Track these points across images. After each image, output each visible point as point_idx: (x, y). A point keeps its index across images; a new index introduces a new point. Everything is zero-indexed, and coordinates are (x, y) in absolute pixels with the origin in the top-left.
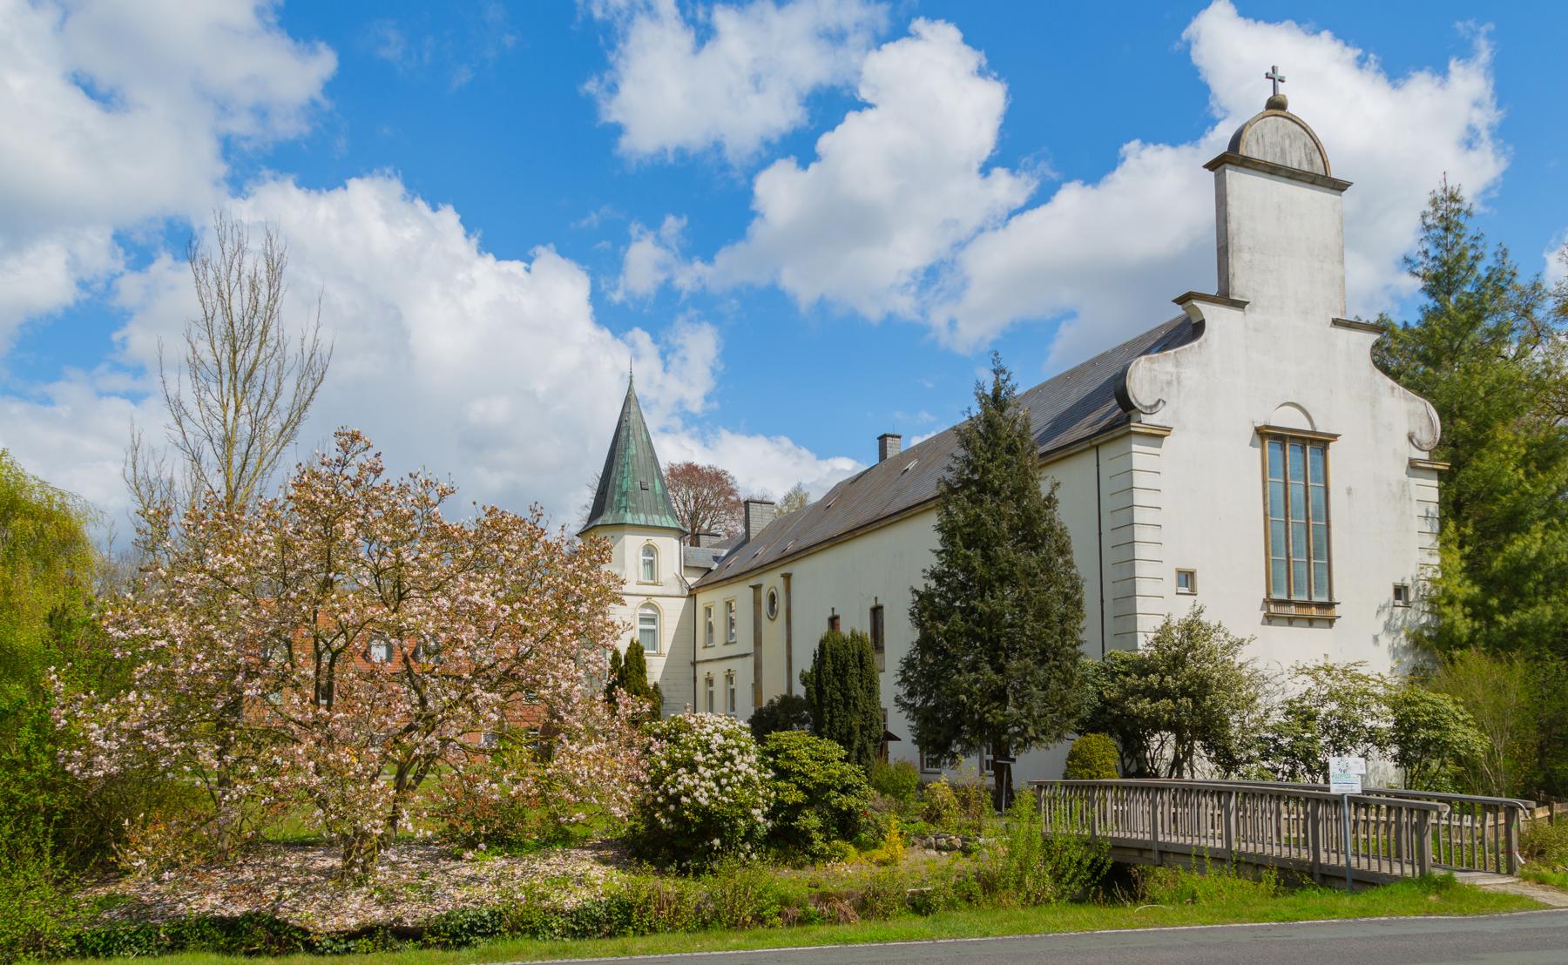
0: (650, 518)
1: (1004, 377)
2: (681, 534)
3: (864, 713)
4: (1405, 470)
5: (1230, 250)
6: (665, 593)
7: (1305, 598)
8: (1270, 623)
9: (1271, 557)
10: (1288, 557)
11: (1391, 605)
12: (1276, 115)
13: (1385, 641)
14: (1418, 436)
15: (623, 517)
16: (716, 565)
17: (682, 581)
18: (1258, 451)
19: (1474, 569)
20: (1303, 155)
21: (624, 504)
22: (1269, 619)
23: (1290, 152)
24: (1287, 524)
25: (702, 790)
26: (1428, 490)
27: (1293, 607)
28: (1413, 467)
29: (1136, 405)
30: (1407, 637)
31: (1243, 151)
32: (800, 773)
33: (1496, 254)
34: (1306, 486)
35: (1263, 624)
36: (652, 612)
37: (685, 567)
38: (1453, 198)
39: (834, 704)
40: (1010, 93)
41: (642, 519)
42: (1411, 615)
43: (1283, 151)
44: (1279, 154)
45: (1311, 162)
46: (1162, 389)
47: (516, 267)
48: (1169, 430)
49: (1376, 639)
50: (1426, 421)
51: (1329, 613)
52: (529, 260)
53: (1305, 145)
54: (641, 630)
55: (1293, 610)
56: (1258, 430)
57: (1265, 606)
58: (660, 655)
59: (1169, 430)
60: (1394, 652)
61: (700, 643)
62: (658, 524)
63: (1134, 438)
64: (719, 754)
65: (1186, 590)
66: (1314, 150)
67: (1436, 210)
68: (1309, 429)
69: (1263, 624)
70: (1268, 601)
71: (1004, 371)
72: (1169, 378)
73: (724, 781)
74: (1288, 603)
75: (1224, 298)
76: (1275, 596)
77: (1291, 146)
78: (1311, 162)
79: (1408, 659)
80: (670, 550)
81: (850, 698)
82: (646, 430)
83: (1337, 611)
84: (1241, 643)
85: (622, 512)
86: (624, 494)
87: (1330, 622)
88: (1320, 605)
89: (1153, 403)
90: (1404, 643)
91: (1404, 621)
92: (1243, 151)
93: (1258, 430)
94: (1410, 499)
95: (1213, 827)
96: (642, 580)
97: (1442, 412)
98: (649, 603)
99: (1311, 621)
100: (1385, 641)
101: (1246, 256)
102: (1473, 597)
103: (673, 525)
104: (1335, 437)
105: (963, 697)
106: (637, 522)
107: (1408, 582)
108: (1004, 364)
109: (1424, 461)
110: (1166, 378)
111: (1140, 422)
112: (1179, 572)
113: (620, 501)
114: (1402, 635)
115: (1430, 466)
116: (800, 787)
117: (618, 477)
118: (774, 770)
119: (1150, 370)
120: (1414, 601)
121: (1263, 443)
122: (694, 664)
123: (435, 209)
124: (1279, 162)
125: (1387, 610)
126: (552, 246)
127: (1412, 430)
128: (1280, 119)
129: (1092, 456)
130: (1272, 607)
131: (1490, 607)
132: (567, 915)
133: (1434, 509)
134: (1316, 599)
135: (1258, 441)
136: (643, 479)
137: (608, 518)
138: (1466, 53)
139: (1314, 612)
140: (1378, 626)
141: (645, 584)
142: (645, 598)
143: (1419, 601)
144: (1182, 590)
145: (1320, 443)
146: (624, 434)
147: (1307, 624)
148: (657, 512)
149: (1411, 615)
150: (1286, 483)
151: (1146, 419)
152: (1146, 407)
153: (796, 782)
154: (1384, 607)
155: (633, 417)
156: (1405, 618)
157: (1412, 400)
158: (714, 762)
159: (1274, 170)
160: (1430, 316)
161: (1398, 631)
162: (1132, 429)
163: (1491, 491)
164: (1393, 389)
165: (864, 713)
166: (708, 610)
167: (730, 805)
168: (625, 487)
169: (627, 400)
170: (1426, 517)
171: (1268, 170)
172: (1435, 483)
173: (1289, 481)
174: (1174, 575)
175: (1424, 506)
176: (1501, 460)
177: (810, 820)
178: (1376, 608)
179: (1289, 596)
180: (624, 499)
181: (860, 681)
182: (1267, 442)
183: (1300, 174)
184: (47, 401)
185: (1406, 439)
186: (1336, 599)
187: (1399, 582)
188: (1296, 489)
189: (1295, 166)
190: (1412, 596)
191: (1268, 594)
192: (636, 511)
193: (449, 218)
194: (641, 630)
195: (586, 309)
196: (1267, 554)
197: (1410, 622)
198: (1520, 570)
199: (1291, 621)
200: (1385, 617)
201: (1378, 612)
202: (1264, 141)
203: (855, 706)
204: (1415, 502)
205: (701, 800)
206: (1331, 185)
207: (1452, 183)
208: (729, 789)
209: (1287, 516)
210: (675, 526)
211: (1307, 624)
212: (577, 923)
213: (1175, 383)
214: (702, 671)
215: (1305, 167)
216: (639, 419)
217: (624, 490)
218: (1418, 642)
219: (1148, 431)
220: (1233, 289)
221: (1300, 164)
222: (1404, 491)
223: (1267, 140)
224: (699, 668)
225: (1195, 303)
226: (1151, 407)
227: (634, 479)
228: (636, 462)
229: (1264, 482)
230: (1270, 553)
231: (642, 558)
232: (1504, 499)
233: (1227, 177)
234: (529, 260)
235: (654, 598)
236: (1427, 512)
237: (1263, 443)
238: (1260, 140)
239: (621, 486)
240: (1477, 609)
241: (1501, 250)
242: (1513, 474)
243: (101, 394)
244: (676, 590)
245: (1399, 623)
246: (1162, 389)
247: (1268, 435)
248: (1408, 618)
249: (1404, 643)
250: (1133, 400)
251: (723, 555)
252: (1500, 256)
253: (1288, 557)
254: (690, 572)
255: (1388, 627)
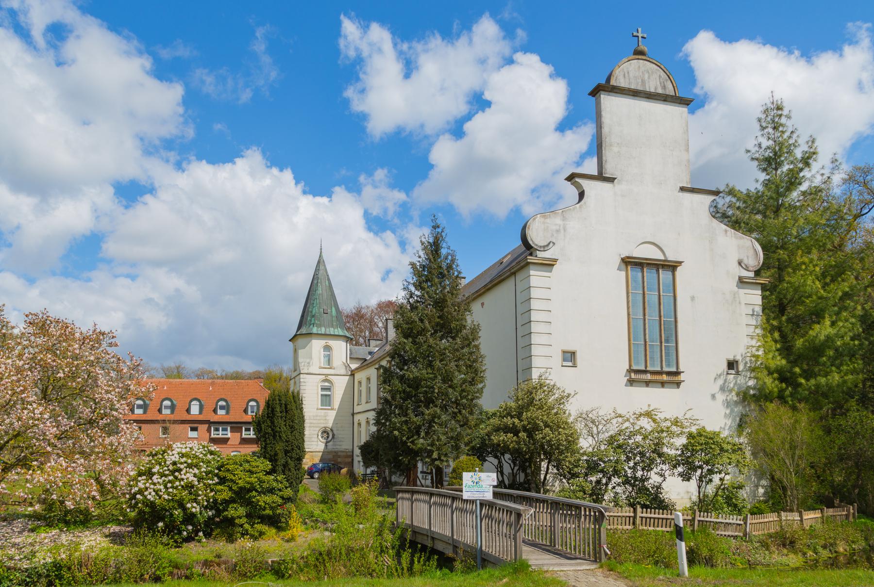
0: (328, 330)
1: (439, 230)
2: (348, 340)
3: (287, 441)
4: (736, 284)
5: (604, 145)
6: (336, 374)
7: (659, 369)
8: (631, 385)
9: (632, 342)
10: (645, 342)
11: (725, 373)
12: (638, 59)
13: (721, 397)
14: (746, 261)
15: (312, 329)
16: (370, 356)
17: (347, 366)
18: (623, 273)
19: (786, 349)
20: (658, 83)
21: (313, 322)
22: (631, 382)
23: (649, 82)
24: (645, 320)
25: (152, 490)
26: (755, 297)
27: (664, 376)
28: (742, 282)
29: (533, 245)
30: (738, 394)
31: (613, 82)
32: (232, 480)
33: (807, 142)
34: (659, 296)
35: (626, 385)
36: (329, 385)
37: (350, 358)
38: (779, 108)
39: (267, 436)
40: (570, 84)
41: (323, 330)
42: (741, 380)
43: (643, 82)
44: (640, 84)
45: (664, 87)
46: (553, 235)
47: (324, 200)
48: (556, 260)
49: (713, 396)
50: (751, 252)
51: (676, 379)
52: (330, 196)
53: (660, 77)
54: (322, 395)
55: (649, 377)
56: (623, 260)
57: (628, 374)
58: (332, 409)
59: (556, 260)
60: (728, 404)
61: (355, 404)
62: (332, 333)
63: (531, 267)
64: (171, 468)
65: (570, 364)
66: (667, 80)
67: (767, 116)
68: (662, 258)
69: (626, 385)
70: (630, 371)
71: (438, 227)
72: (558, 228)
73: (169, 485)
74: (645, 372)
75: (601, 177)
76: (635, 367)
77: (649, 78)
78: (664, 87)
79: (739, 409)
80: (340, 349)
81: (276, 432)
82: (329, 279)
83: (682, 377)
84: (569, 396)
85: (311, 326)
86: (313, 316)
87: (678, 384)
88: (669, 373)
89: (546, 244)
90: (735, 398)
91: (735, 384)
92: (613, 82)
93: (623, 260)
94: (740, 303)
95: (535, 521)
96: (322, 366)
97: (764, 248)
98: (326, 379)
99: (663, 384)
100: (721, 397)
101: (615, 149)
102: (782, 367)
103: (341, 333)
104: (681, 263)
105: (396, 433)
106: (320, 332)
107: (739, 358)
108: (438, 222)
109: (749, 278)
110: (554, 228)
111: (536, 256)
112: (564, 352)
113: (311, 320)
114: (734, 393)
115: (754, 281)
116: (230, 489)
117: (311, 307)
118: (218, 478)
119: (544, 223)
120: (742, 371)
121: (627, 268)
122: (353, 414)
123: (281, 170)
124: (640, 88)
125: (722, 377)
126: (343, 186)
127: (741, 258)
128: (641, 61)
129: (513, 277)
130: (633, 375)
131: (795, 373)
132: (23, 571)
133: (758, 309)
134: (666, 369)
135: (623, 266)
136: (325, 307)
137: (304, 330)
138: (853, 41)
139: (665, 378)
140: (716, 388)
141: (325, 368)
142: (324, 376)
143: (746, 371)
144: (565, 364)
145: (672, 267)
146: (315, 282)
147: (645, 385)
148: (332, 326)
149: (741, 380)
150: (644, 294)
151: (540, 254)
152: (541, 247)
153: (228, 486)
154: (720, 375)
155: (321, 272)
156: (736, 382)
157: (741, 238)
158: (167, 472)
159: (635, 94)
160: (767, 184)
161: (731, 391)
162: (529, 261)
163: (800, 297)
164: (726, 231)
165: (287, 441)
166: (360, 383)
167: (168, 501)
168: (314, 312)
169: (319, 262)
170: (753, 315)
171: (631, 93)
172: (760, 292)
173: (646, 292)
174: (560, 355)
175: (751, 307)
176: (802, 276)
177: (237, 511)
178: (714, 376)
179: (646, 367)
180: (313, 319)
181: (285, 421)
182: (629, 267)
183: (655, 95)
184: (89, 280)
185: (737, 264)
186: (681, 369)
187: (731, 358)
188: (652, 297)
189: (652, 90)
190: (741, 367)
191: (630, 366)
192: (319, 326)
193: (288, 176)
194: (322, 395)
195: (361, 222)
196: (629, 340)
197: (739, 385)
198: (817, 350)
199: (647, 383)
200: (720, 382)
201: (715, 379)
202: (629, 76)
203: (280, 437)
204: (743, 306)
205: (149, 497)
206: (679, 101)
207: (777, 97)
208: (171, 490)
209: (644, 315)
210: (343, 334)
211: (660, 385)
212: (28, 576)
213: (562, 231)
214: (357, 418)
215: (660, 91)
216: (325, 273)
217: (313, 314)
218: (745, 397)
219: (540, 262)
220: (606, 170)
221: (656, 89)
222: (734, 298)
223: (631, 75)
224: (355, 416)
225: (577, 180)
226: (544, 247)
227: (320, 307)
228: (321, 299)
229: (628, 293)
230: (632, 339)
231: (322, 353)
232: (808, 301)
233: (602, 99)
234: (330, 196)
235: (329, 376)
236: (753, 311)
237: (627, 268)
238: (626, 75)
239: (311, 312)
240: (784, 377)
241: (812, 139)
242: (813, 285)
243: (116, 277)
244: (343, 371)
245: (732, 385)
246: (553, 235)
247: (628, 262)
248: (738, 381)
249: (735, 398)
250: (531, 242)
251: (375, 351)
252: (810, 143)
253: (645, 342)
254: (354, 361)
255: (722, 389)
